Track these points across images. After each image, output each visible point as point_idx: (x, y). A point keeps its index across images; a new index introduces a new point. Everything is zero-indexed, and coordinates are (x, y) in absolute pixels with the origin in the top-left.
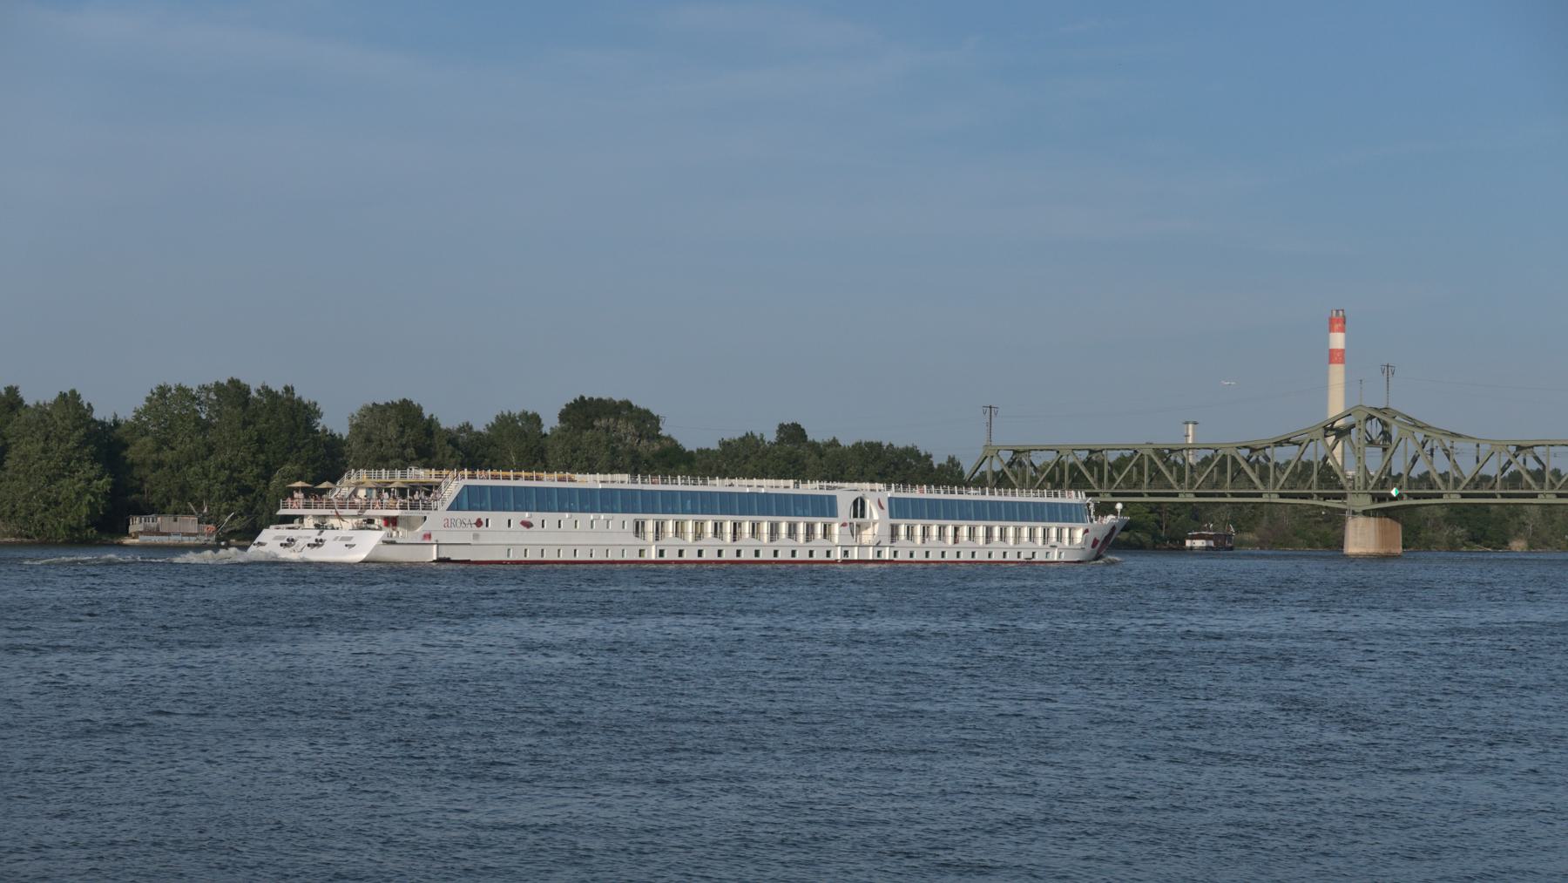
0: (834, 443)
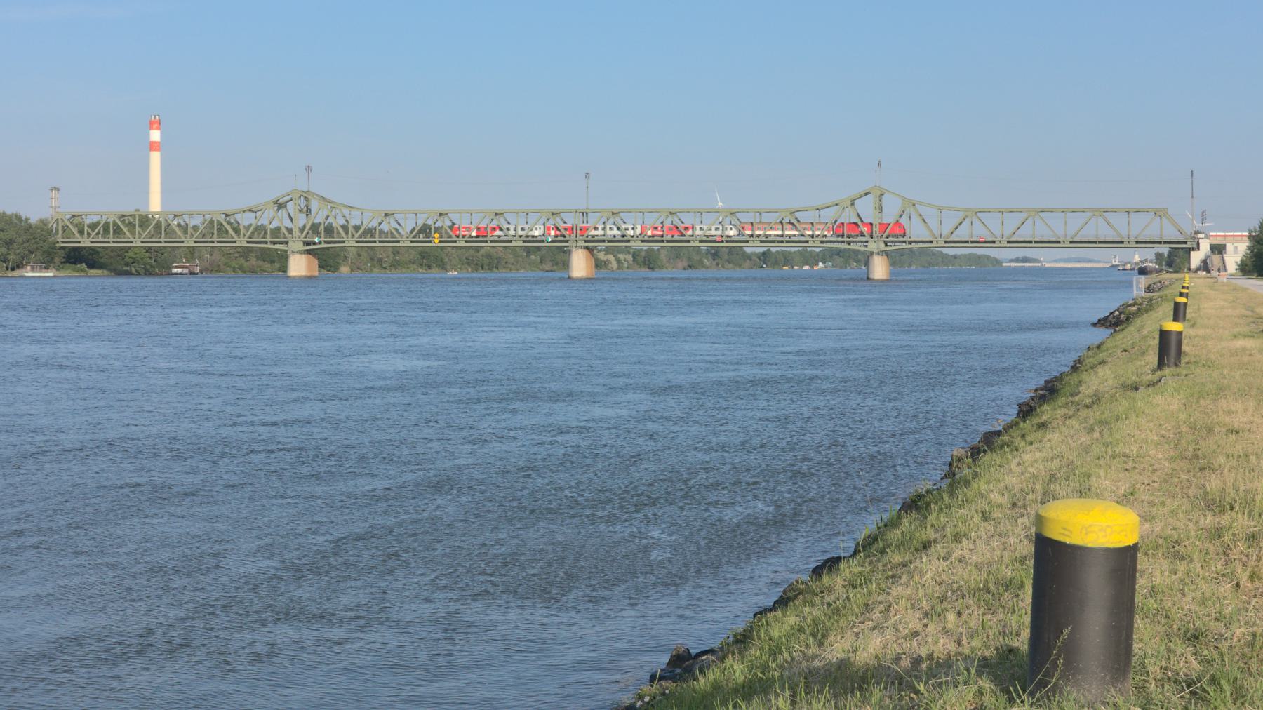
0: (27, 219)
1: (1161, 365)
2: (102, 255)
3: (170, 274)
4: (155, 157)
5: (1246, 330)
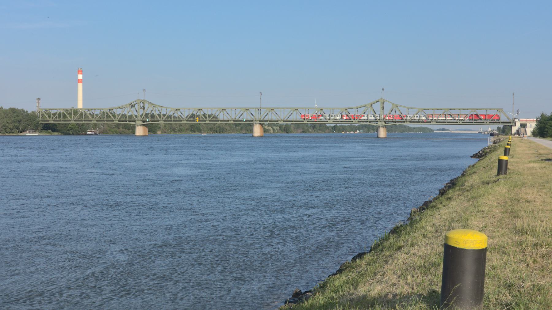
0: (27, 112)
1: (499, 174)
2: (59, 126)
3: (86, 134)
4: (80, 86)
5: (534, 159)
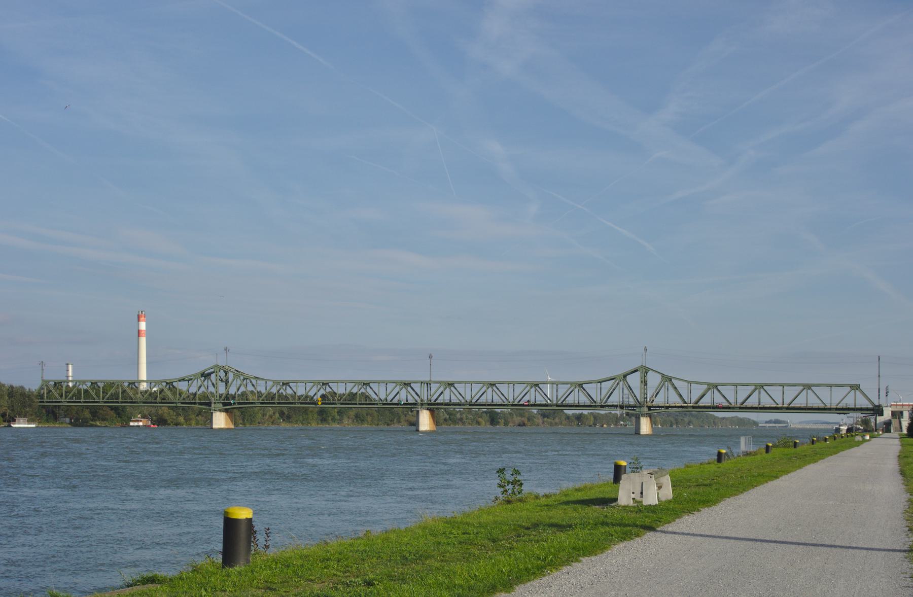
4: (143, 340)
